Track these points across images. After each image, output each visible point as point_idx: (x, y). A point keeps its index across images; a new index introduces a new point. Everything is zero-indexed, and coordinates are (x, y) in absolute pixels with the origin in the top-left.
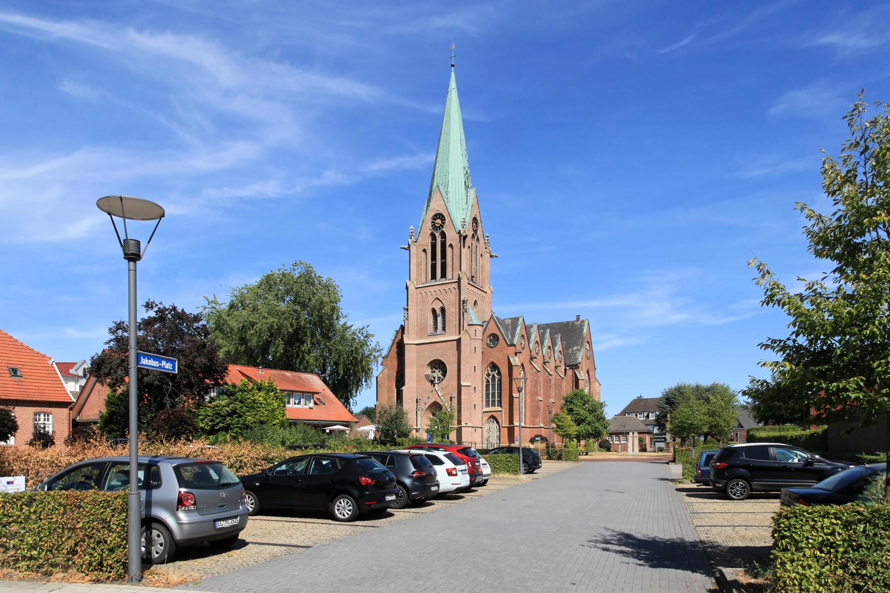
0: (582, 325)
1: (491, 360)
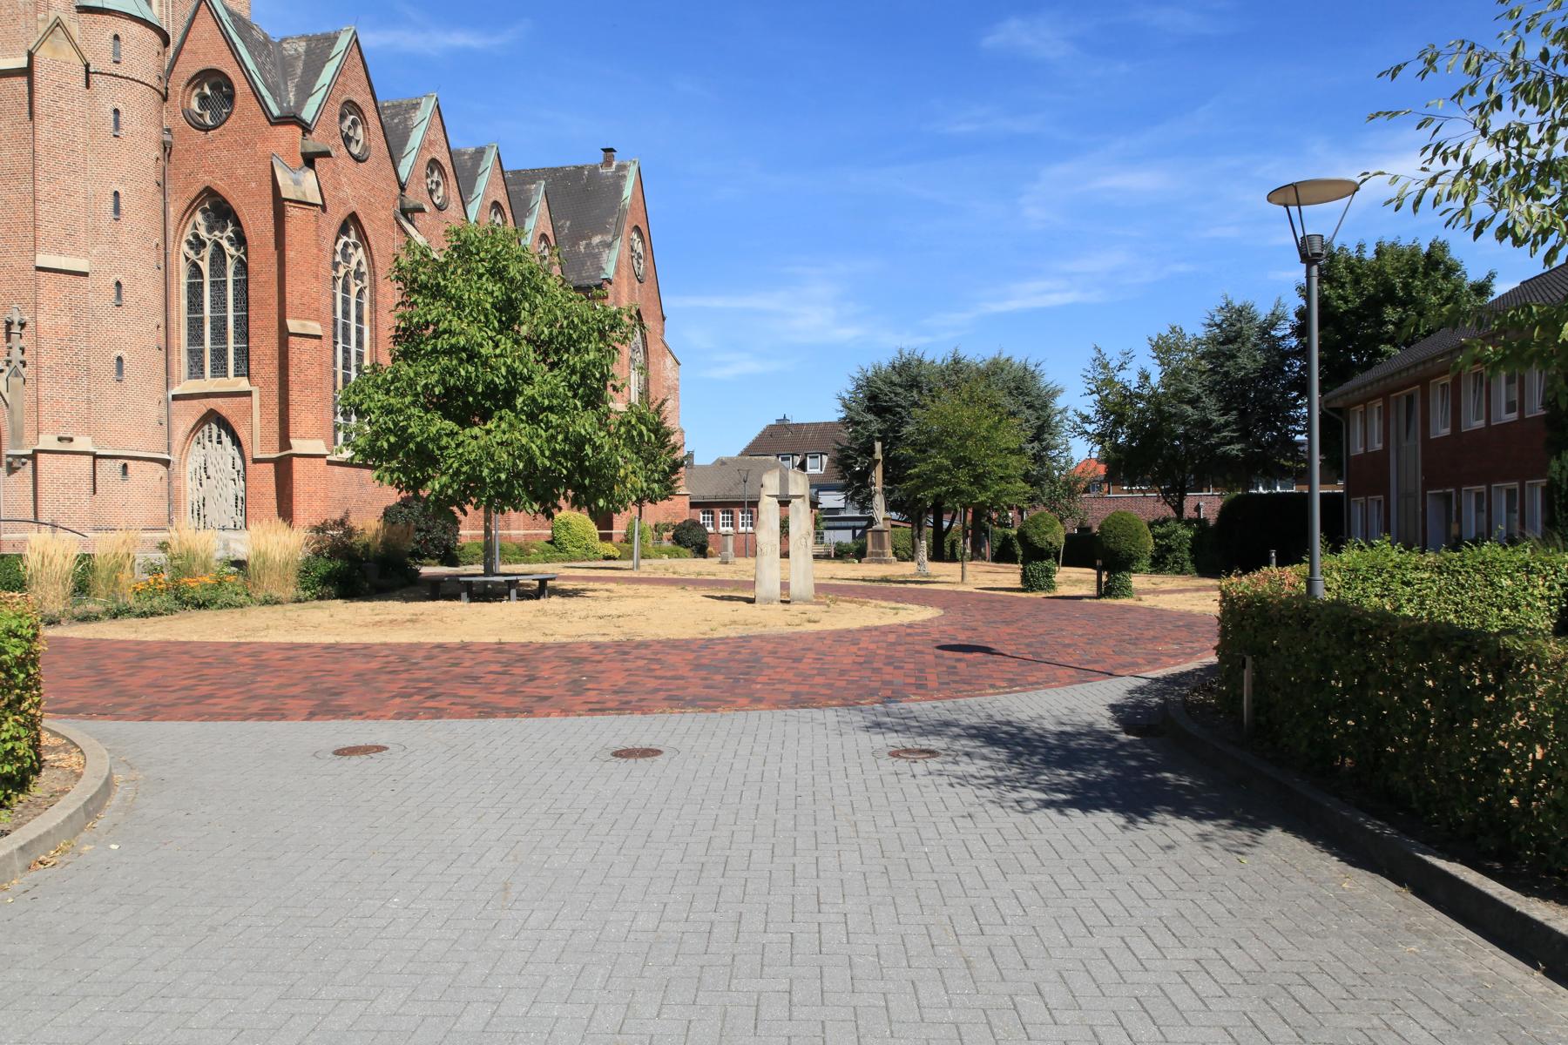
0: (619, 178)
1: (205, 180)
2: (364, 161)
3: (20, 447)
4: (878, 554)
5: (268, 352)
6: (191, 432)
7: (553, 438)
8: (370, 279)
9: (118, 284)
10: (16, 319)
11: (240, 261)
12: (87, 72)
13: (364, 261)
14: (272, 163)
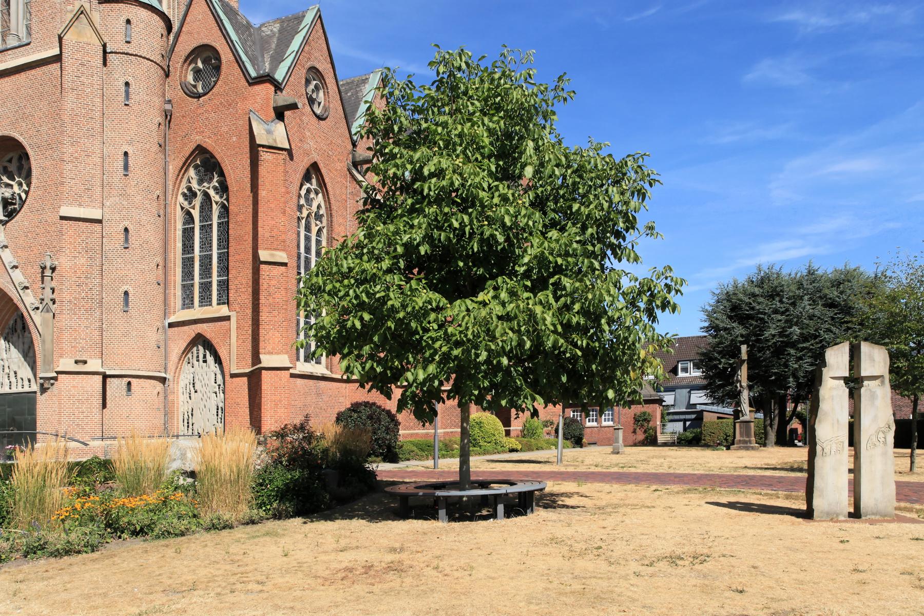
2: (324, 119)
4: (746, 442)
5: (244, 282)
6: (183, 353)
7: (567, 308)
8: (328, 220)
9: (126, 230)
10: (48, 265)
12: (105, 52)
13: (323, 205)
14: (249, 118)
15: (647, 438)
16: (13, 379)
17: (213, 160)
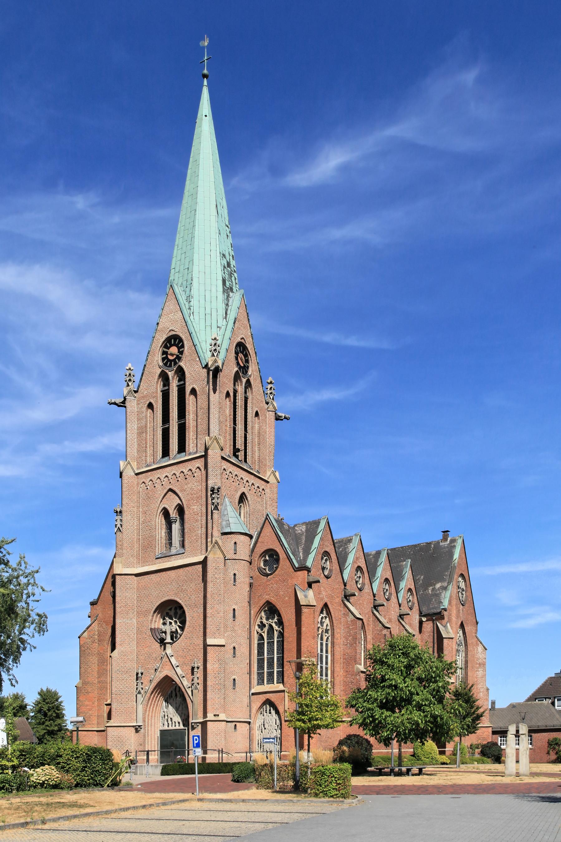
0: (452, 547)
1: (266, 598)
3: (197, 719)
7: (426, 716)
8: (331, 632)
9: (234, 648)
10: (196, 665)
11: (280, 632)
13: (329, 624)
15: (558, 758)
16: (170, 722)
17: (274, 608)
